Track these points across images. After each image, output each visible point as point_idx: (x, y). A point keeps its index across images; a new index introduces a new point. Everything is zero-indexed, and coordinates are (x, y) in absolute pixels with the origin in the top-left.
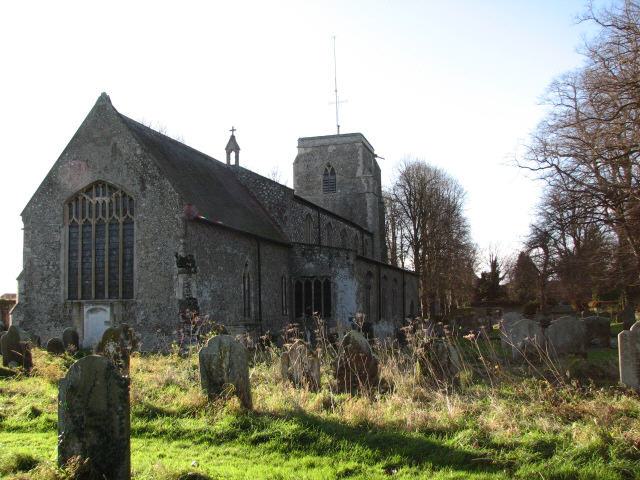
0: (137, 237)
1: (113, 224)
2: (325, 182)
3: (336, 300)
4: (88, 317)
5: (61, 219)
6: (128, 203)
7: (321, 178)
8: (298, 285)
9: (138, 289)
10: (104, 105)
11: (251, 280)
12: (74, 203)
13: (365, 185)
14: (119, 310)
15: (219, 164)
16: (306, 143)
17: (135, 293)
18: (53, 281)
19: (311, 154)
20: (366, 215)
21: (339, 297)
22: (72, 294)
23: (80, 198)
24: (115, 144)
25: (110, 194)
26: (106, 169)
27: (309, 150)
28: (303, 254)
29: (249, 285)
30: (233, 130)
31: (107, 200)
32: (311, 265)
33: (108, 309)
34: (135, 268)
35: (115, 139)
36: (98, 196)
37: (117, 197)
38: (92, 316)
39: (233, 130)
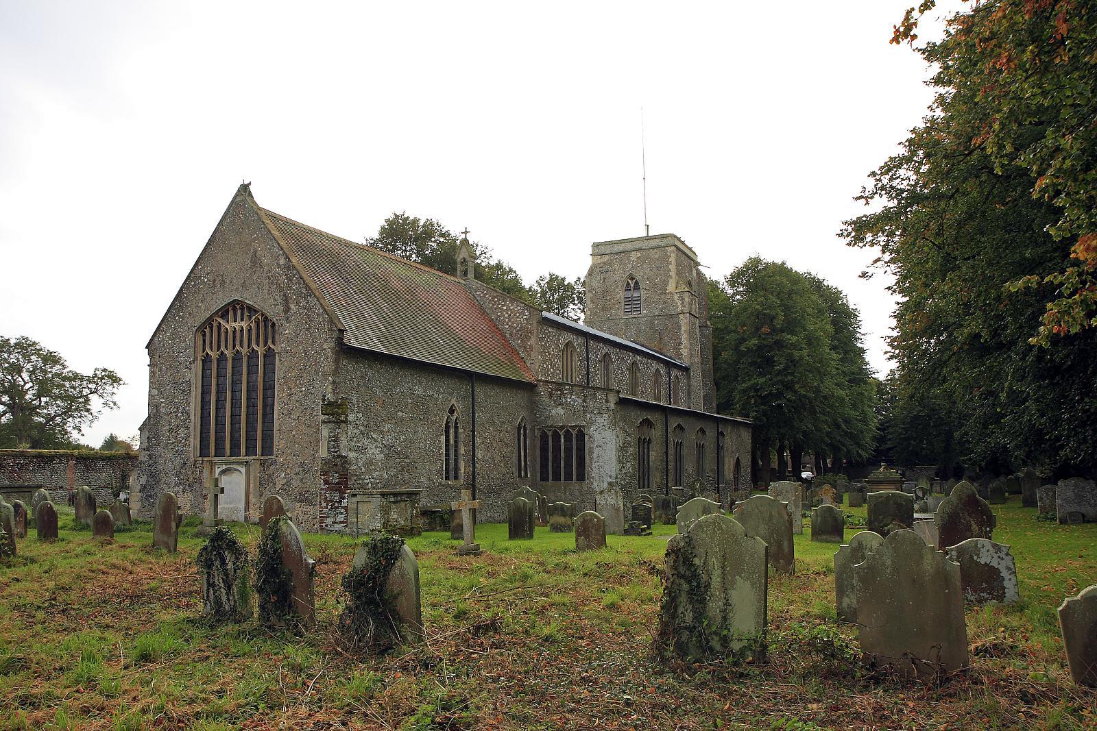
0: (279, 374)
1: (253, 355)
5: (192, 350)
6: (268, 327)
7: (621, 295)
8: (544, 437)
9: (279, 443)
11: (460, 430)
12: (207, 331)
13: (679, 302)
14: (256, 468)
16: (602, 250)
17: (275, 449)
18: (182, 434)
19: (609, 263)
20: (680, 343)
21: (595, 455)
22: (204, 451)
23: (215, 324)
24: (255, 252)
25: (250, 318)
26: (244, 285)
27: (606, 258)
28: (551, 395)
29: (456, 437)
30: (466, 232)
31: (244, 325)
32: (560, 411)
33: (243, 470)
34: (276, 416)
36: (235, 321)
37: (257, 323)
39: (466, 232)
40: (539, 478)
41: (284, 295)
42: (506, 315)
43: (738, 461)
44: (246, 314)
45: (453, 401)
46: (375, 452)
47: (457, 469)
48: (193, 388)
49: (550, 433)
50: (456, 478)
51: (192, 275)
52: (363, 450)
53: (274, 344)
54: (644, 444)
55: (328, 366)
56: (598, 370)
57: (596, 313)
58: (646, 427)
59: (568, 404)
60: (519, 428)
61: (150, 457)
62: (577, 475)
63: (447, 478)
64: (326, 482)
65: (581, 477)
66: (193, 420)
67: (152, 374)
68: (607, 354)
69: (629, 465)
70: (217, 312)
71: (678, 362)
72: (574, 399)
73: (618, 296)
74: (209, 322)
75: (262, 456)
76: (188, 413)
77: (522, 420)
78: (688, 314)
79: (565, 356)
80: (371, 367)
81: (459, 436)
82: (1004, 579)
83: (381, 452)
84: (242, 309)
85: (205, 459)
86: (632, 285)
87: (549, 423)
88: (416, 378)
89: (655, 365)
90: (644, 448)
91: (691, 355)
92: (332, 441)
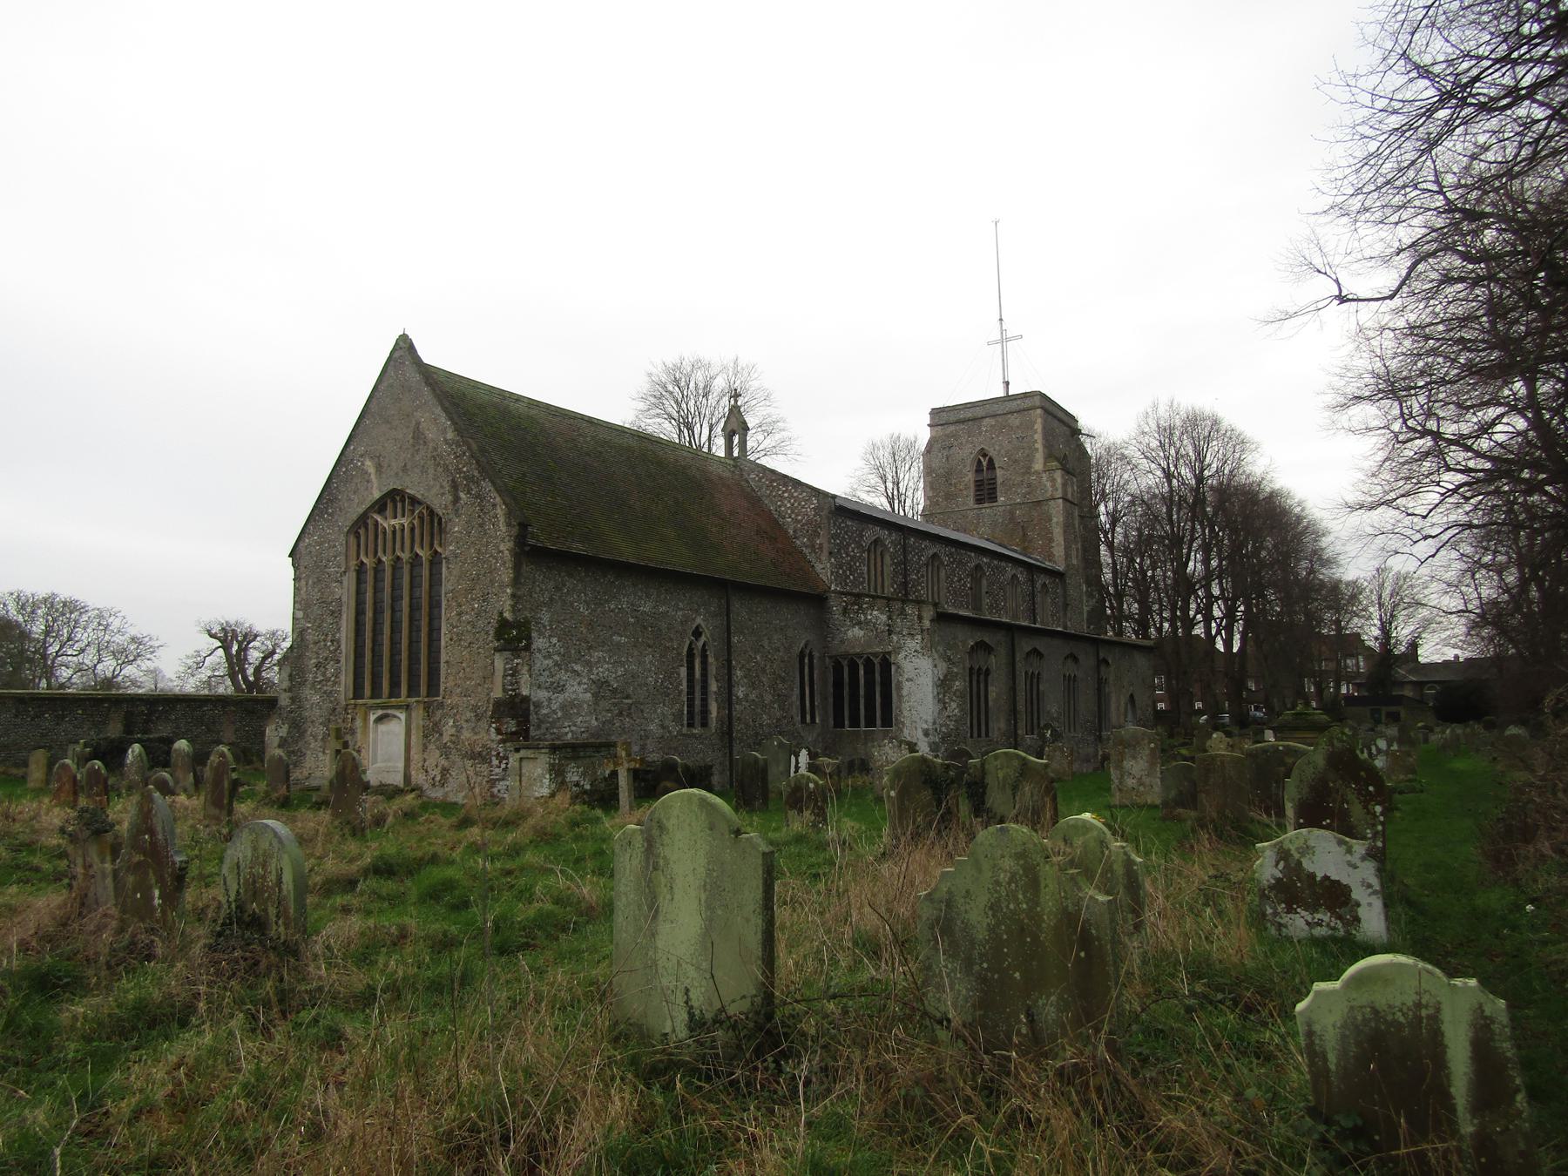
0: (446, 586)
1: (416, 560)
2: (979, 485)
3: (900, 696)
4: (376, 731)
5: (343, 558)
6: (433, 524)
7: (970, 477)
9: (445, 682)
10: (404, 349)
11: (711, 660)
12: (362, 531)
13: (1049, 484)
14: (418, 714)
15: (669, 443)
16: (945, 417)
17: (442, 688)
19: (955, 436)
20: (1051, 540)
21: (905, 692)
22: (358, 692)
24: (418, 424)
25: (413, 512)
26: (405, 469)
31: (405, 521)
32: (856, 632)
33: (403, 716)
35: (418, 414)
36: (395, 517)
37: (421, 518)
38: (382, 728)
40: (831, 722)
41: (453, 481)
42: (789, 505)
43: (1132, 696)
44: (407, 507)
45: (699, 620)
46: (577, 690)
47: (705, 712)
48: (344, 609)
49: (845, 663)
50: (705, 724)
51: (344, 458)
52: (559, 688)
53: (440, 545)
54: (978, 677)
55: (506, 575)
56: (923, 576)
57: (937, 503)
58: (1069, 661)
59: (867, 622)
60: (802, 655)
61: (293, 700)
62: (882, 720)
63: (690, 725)
64: (498, 731)
65: (888, 721)
66: (344, 651)
67: (297, 590)
68: (935, 556)
69: (954, 705)
70: (372, 506)
71: (1048, 565)
72: (878, 616)
73: (967, 479)
74: (363, 520)
75: (427, 696)
76: (338, 641)
77: (806, 645)
78: (1061, 501)
79: (872, 557)
80: (570, 575)
81: (709, 668)
82: (1358, 905)
83: (586, 691)
84: (403, 501)
85: (360, 701)
86: (985, 463)
87: (842, 649)
88: (641, 590)
89: (1010, 570)
90: (978, 682)
91: (1068, 556)
92: (510, 675)
